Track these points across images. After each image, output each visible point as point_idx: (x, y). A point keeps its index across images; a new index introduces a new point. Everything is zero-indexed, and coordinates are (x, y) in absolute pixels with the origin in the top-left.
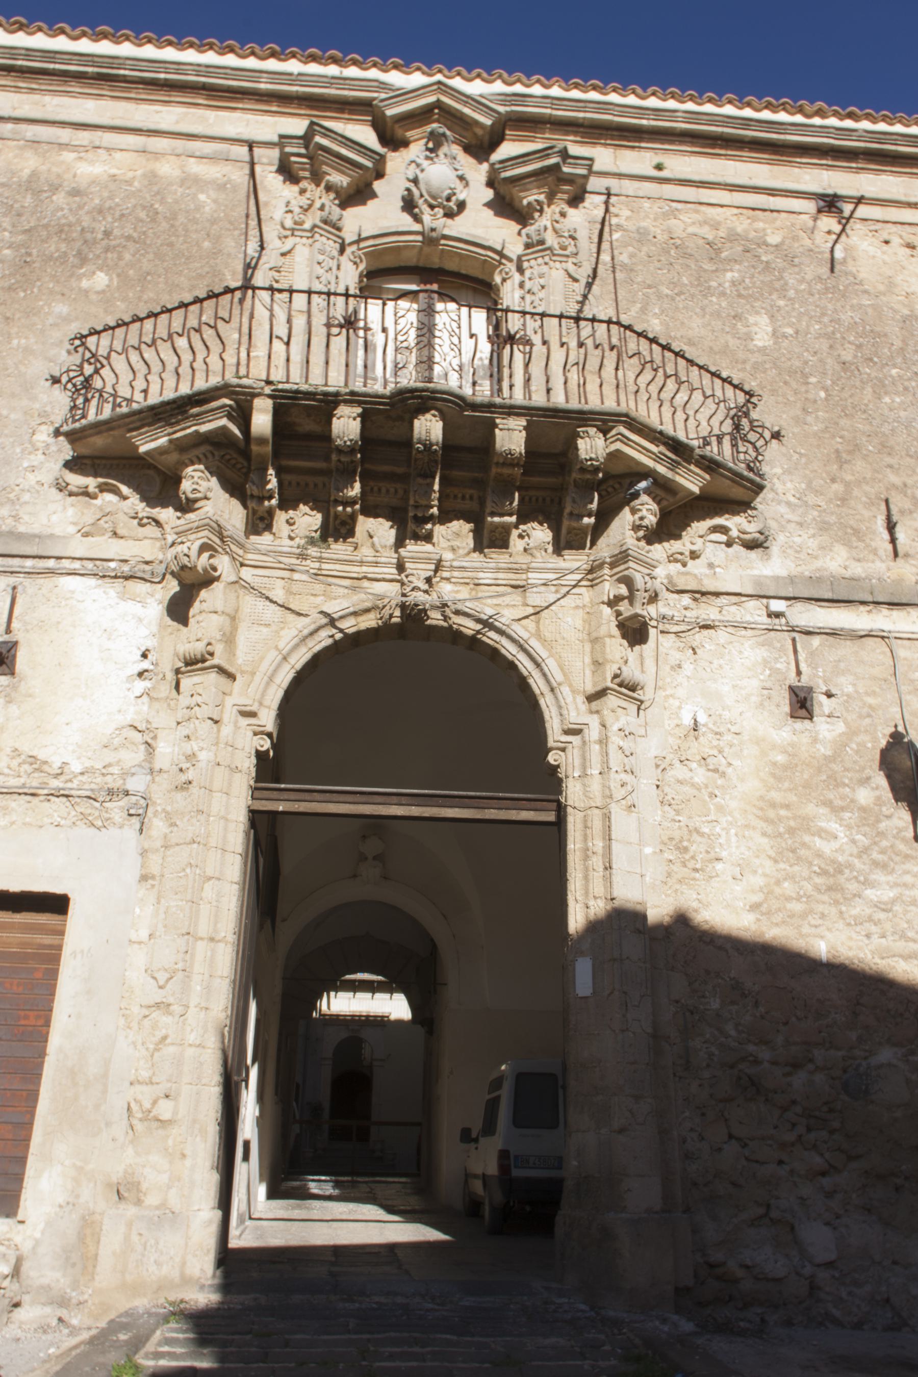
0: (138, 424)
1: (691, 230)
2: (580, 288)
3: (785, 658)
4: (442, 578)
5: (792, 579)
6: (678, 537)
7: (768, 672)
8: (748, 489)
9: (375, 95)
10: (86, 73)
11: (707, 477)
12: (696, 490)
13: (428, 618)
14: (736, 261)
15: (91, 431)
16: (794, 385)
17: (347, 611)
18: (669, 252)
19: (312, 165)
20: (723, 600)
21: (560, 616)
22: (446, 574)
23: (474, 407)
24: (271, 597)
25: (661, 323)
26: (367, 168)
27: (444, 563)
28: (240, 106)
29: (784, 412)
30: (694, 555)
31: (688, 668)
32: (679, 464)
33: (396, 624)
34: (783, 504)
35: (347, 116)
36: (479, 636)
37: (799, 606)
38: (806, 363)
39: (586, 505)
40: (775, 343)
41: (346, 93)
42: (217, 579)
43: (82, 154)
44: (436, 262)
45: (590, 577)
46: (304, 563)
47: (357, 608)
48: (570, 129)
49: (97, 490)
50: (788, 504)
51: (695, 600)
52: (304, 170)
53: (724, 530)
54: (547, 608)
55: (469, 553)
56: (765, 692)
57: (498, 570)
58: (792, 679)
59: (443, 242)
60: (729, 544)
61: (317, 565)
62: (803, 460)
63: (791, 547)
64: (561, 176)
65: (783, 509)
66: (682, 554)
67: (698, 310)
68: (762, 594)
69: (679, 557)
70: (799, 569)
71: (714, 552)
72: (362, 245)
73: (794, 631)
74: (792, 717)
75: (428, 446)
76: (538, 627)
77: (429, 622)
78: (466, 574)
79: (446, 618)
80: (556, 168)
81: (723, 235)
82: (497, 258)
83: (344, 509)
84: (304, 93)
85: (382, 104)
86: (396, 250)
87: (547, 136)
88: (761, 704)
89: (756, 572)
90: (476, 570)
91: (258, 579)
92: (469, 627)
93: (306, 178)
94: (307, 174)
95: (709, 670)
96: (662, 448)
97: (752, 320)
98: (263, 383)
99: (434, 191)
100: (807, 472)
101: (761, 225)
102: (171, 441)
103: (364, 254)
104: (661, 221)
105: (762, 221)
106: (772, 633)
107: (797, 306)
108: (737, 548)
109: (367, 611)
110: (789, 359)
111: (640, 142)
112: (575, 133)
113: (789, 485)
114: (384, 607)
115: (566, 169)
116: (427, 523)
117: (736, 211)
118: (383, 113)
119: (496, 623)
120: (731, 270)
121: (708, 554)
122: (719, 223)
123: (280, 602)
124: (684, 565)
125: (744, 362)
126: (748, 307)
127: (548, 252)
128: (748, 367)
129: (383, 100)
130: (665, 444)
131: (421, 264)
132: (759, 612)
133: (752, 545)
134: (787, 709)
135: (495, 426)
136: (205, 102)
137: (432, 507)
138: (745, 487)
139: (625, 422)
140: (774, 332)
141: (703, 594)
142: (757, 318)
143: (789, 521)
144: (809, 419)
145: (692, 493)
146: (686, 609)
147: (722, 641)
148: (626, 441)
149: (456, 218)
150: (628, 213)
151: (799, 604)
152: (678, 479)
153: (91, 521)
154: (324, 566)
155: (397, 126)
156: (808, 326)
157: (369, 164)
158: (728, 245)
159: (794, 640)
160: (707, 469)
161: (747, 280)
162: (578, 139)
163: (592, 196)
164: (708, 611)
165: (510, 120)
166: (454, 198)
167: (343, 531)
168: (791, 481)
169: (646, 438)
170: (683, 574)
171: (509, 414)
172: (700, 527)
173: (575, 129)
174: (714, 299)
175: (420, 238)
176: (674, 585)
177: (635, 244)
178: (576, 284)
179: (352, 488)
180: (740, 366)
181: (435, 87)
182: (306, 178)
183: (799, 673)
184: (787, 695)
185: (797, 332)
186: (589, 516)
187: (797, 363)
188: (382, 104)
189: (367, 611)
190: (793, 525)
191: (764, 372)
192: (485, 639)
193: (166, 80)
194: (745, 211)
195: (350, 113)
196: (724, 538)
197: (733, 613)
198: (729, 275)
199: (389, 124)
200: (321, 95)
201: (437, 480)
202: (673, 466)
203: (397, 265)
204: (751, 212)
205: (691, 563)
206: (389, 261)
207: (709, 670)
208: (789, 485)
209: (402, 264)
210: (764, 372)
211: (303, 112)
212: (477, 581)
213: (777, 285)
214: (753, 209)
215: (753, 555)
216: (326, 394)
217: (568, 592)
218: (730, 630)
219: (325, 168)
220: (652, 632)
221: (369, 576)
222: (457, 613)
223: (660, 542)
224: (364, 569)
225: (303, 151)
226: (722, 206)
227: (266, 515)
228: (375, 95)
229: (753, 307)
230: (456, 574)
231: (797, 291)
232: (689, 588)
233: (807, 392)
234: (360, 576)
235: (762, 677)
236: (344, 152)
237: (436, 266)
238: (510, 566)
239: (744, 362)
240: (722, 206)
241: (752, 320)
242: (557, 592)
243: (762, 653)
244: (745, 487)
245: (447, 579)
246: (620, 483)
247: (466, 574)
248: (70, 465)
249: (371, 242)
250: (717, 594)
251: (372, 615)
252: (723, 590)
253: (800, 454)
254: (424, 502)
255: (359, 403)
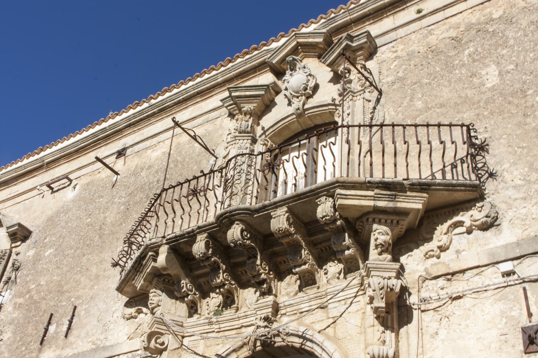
0: (133, 276)
1: (441, 37)
2: (371, 105)
3: (518, 306)
4: (282, 315)
5: (518, 244)
6: (430, 239)
7: (504, 320)
8: (465, 191)
9: (266, 57)
10: (155, 112)
11: (425, 195)
12: (420, 206)
13: (275, 342)
14: (471, 41)
15: (123, 286)
16: (516, 101)
17: (229, 350)
18: (428, 57)
19: (238, 107)
20: (468, 274)
21: (347, 320)
22: (283, 312)
23: (257, 211)
24: (197, 351)
25: (423, 103)
26: (263, 95)
27: (280, 305)
28: (214, 93)
29: (509, 123)
30: (443, 249)
31: (443, 333)
32: (396, 195)
33: (259, 351)
34: (510, 189)
35: (258, 73)
36: (303, 347)
37: (527, 261)
38: (525, 82)
39: (341, 244)
40: (501, 80)
41: (253, 63)
42: (165, 349)
43: (154, 149)
44: (311, 124)
45: (362, 288)
46: (212, 327)
47: (234, 347)
48: (364, 19)
49: (136, 314)
50: (515, 187)
51: (448, 280)
52: (235, 110)
53: (460, 224)
54: (341, 316)
55: (296, 294)
56: (503, 337)
57: (310, 300)
58: (525, 322)
59: (306, 113)
60: (469, 232)
61: (218, 326)
62: (525, 151)
63: (518, 218)
64: (353, 49)
65: (511, 192)
66: (433, 251)
67: (446, 83)
68: (495, 261)
69: (432, 253)
70: (526, 233)
71: (460, 241)
72: (267, 134)
73: (524, 282)
74: (526, 353)
75: (235, 243)
76: (335, 331)
77: (276, 345)
78: (293, 308)
79: (284, 340)
80: (347, 47)
81: (462, 29)
82: (334, 107)
83: (220, 290)
84: (236, 73)
85: (269, 60)
86: (286, 127)
87: (354, 29)
88: (500, 348)
89: (491, 246)
90: (298, 304)
91: (191, 343)
92: (296, 342)
93: (237, 114)
94: (237, 111)
95: (458, 331)
96: (377, 191)
97: (484, 72)
98: (161, 239)
99: (296, 90)
100: (529, 158)
101: (488, 10)
102: (144, 281)
103: (269, 138)
104: (422, 41)
105: (489, 7)
106: (507, 289)
107: (516, 48)
108: (476, 233)
109: (241, 347)
110: (512, 86)
111: (406, 4)
112: (369, 20)
113: (516, 173)
114: (249, 342)
115: (354, 45)
116: (263, 284)
117: (470, 11)
118: (272, 63)
119: (307, 336)
120: (468, 48)
121: (458, 244)
122: (459, 24)
123: (201, 354)
124: (438, 257)
125: (479, 102)
126: (481, 65)
127: (350, 93)
128: (482, 104)
129: (269, 58)
130: (377, 188)
131: (305, 128)
132: (495, 276)
133: (485, 227)
134: (521, 348)
135: (271, 217)
136: (200, 99)
137: (261, 274)
138: (461, 190)
139: (339, 186)
140: (500, 74)
141: (453, 274)
142: (488, 69)
143: (516, 199)
144: (529, 120)
145: (418, 210)
146: (442, 289)
147: (468, 306)
148: (346, 197)
149: (314, 97)
150: (402, 47)
151: (527, 260)
152: (399, 205)
153: (133, 331)
154: (222, 326)
155: (282, 65)
156: (524, 57)
157: (263, 93)
158: (466, 33)
159: (524, 289)
160: (422, 190)
161: (479, 49)
162: (372, 21)
163: (381, 48)
164: (458, 286)
165: (332, 32)
166: (308, 88)
167: (228, 302)
168: (517, 169)
169: (361, 189)
170: (438, 263)
171: (277, 207)
172: (442, 229)
173: (367, 18)
174: (457, 71)
175: (294, 116)
176: (430, 275)
177: (406, 62)
178: (370, 103)
179: (219, 278)
180: (476, 106)
181: (294, 37)
182: (237, 114)
183: (530, 315)
184: (520, 336)
185: (517, 66)
186: (348, 248)
187: (517, 86)
188: (269, 60)
189: (241, 347)
190: (518, 201)
191: (494, 102)
192: (306, 348)
193: (183, 98)
194: (477, 7)
195: (259, 71)
196: (463, 229)
197: (473, 281)
198: (467, 52)
199: (278, 66)
200: (240, 72)
201: (259, 257)
202: (393, 198)
203: (293, 134)
204: (481, 6)
205: (443, 254)
206: (287, 134)
207: (458, 331)
208: (516, 173)
209: (296, 132)
210: (494, 102)
211: (240, 82)
212: (300, 311)
213: (500, 42)
214: (482, 4)
215: (489, 234)
216: (188, 233)
217: (351, 303)
218: (474, 296)
219: (242, 105)
220: (415, 313)
221: (244, 324)
222: (288, 334)
223: (417, 248)
224: (241, 321)
225: (232, 102)
226: (461, 13)
227: (193, 305)
228: (266, 57)
229: (484, 64)
230: (288, 310)
231: (515, 39)
232: (440, 273)
233: (526, 102)
234: (239, 326)
235: (500, 326)
236: (248, 93)
237: (301, 130)
238: (316, 295)
239: (479, 102)
240: (461, 13)
241: (484, 72)
242: (345, 304)
243: (500, 306)
244: (461, 190)
245: (285, 314)
246: (362, 222)
247: (293, 308)
248: (128, 305)
249: (271, 130)
250: (463, 271)
251: (245, 349)
252: (465, 267)
253: (523, 148)
254: (255, 273)
255: (205, 231)
